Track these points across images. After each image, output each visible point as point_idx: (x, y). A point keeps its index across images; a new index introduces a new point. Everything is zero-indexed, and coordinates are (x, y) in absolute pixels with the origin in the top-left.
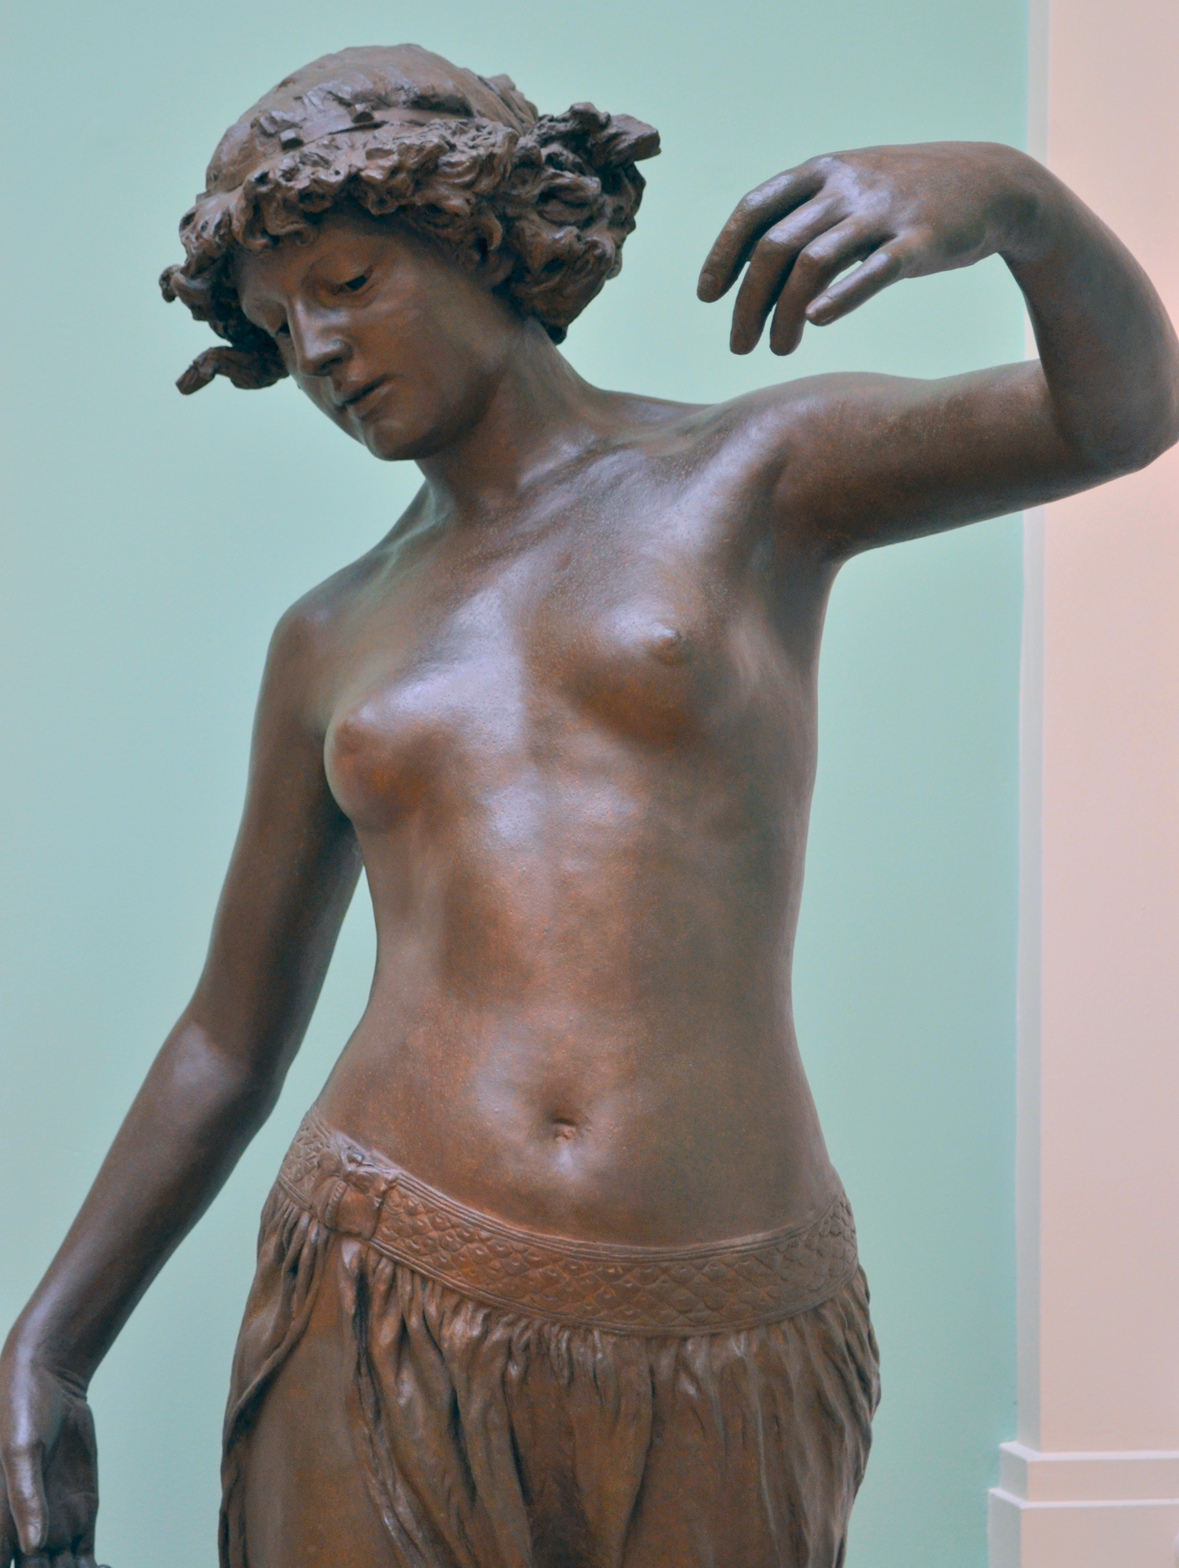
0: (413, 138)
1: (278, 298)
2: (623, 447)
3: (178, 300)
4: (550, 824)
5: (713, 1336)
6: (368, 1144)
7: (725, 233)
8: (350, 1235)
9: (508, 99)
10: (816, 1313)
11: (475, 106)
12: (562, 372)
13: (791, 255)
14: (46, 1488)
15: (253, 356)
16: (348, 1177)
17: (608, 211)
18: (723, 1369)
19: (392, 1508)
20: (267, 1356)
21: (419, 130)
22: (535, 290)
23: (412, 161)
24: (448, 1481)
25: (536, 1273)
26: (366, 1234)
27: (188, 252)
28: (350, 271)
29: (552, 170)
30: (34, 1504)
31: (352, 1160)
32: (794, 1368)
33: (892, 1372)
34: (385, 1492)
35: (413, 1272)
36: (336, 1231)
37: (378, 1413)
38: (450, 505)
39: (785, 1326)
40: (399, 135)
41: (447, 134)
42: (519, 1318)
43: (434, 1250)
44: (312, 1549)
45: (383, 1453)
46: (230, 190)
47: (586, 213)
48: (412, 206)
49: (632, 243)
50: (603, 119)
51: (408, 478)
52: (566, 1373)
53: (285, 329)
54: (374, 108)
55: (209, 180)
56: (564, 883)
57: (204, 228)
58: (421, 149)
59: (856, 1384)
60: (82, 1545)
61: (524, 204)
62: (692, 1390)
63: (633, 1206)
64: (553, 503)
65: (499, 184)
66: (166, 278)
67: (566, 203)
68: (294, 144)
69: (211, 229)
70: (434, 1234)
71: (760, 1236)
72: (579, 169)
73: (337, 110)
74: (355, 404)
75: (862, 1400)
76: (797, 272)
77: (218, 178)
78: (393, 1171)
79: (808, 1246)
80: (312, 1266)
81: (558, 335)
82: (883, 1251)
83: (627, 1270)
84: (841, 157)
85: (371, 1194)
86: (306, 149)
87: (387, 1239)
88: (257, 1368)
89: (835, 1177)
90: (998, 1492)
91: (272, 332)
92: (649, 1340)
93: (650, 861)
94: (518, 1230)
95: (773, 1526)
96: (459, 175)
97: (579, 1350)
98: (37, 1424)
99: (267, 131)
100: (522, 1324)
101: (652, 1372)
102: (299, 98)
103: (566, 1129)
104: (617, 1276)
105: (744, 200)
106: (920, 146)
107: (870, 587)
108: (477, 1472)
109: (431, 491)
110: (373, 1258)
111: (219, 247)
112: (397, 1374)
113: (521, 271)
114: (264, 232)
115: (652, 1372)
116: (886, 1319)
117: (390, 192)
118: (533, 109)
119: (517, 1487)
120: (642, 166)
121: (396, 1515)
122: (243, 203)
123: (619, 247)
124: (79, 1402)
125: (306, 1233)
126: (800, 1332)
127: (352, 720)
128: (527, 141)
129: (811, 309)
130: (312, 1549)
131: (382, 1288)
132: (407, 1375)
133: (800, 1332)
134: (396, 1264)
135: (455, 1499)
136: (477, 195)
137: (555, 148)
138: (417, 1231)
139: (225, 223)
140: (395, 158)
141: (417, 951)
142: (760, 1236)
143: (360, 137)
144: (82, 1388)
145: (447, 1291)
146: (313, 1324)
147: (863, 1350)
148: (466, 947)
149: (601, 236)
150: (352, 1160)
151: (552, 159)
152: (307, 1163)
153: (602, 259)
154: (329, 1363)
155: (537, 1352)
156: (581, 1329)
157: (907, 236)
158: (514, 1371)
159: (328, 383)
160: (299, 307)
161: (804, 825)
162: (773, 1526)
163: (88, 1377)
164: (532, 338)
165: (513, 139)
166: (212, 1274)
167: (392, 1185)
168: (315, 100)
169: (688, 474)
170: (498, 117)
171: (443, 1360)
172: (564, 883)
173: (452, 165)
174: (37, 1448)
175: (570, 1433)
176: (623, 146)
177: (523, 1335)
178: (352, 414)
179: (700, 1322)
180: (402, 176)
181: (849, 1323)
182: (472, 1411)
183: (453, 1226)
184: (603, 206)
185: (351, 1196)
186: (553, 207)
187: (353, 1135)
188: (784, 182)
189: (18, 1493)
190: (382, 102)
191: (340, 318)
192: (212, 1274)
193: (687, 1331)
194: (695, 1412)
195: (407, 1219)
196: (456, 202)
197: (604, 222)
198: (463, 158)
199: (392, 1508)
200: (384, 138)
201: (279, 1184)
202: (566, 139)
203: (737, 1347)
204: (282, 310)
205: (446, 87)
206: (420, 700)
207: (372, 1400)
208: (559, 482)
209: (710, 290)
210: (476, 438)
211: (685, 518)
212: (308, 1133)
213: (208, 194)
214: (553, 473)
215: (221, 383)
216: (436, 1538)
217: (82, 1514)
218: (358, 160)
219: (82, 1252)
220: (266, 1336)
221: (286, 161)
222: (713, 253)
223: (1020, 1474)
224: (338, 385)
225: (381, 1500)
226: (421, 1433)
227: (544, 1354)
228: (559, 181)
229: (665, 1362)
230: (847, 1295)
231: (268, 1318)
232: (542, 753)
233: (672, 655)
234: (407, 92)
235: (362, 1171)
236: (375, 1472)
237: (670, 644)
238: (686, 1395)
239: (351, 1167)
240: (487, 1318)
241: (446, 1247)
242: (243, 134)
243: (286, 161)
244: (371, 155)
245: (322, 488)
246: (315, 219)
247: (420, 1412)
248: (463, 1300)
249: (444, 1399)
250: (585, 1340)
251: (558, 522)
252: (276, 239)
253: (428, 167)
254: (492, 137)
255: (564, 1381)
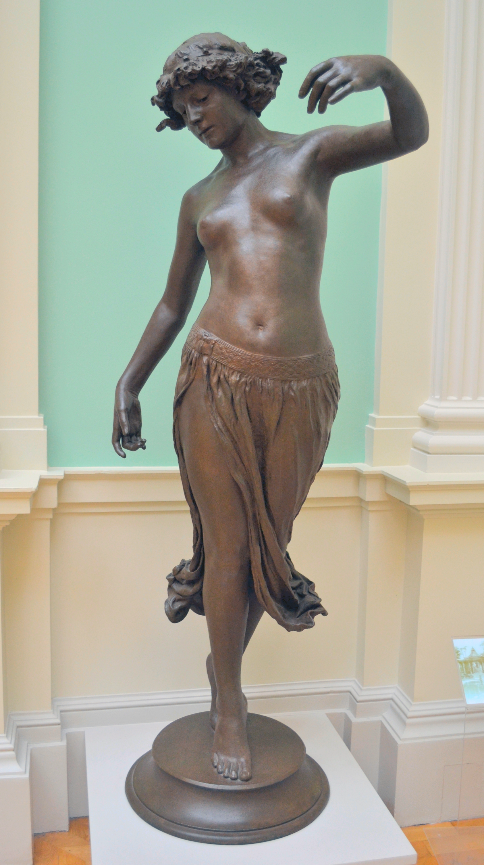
0: (220, 58)
1: (183, 104)
2: (276, 146)
3: (156, 105)
4: (256, 247)
5: (298, 380)
6: (210, 331)
7: (306, 79)
8: (205, 354)
9: (245, 48)
10: (325, 375)
11: (236, 49)
12: (259, 124)
13: (324, 85)
14: (129, 419)
15: (176, 121)
16: (204, 340)
17: (273, 79)
18: (301, 389)
19: (216, 423)
20: (184, 386)
21: (221, 56)
22: (253, 102)
23: (219, 64)
24: (231, 417)
25: (253, 364)
26: (209, 354)
27: (158, 91)
28: (203, 96)
29: (257, 68)
30: (126, 423)
31: (205, 336)
32: (319, 389)
33: (343, 391)
34: (215, 419)
35: (221, 364)
36: (202, 354)
37: (213, 399)
38: (230, 162)
39: (317, 378)
40: (215, 57)
41: (229, 57)
42: (249, 376)
43: (227, 358)
44: (196, 433)
45: (214, 409)
46: (170, 73)
47: (267, 80)
48: (219, 77)
49: (279, 88)
50: (271, 53)
51: (218, 155)
52: (261, 389)
53: (185, 113)
54: (209, 50)
55: (164, 71)
56: (260, 263)
57: (163, 84)
58: (222, 60)
59: (334, 394)
60: (138, 434)
61: (250, 77)
62: (293, 394)
63: (279, 347)
64: (258, 161)
65: (243, 71)
66: (152, 99)
67: (261, 77)
68: (187, 60)
69: (165, 84)
70: (227, 354)
71: (311, 355)
72: (265, 67)
73: (198, 50)
74: (204, 134)
75: (336, 398)
76: (326, 90)
77: (166, 70)
78: (216, 338)
79: (323, 358)
80: (196, 363)
81: (259, 115)
82: (341, 361)
83: (277, 363)
84: (338, 58)
85: (211, 344)
86: (190, 61)
87: (215, 356)
88: (182, 389)
89: (330, 341)
90: (368, 426)
91: (181, 114)
92: (282, 381)
93: (283, 257)
94: (249, 353)
95: (313, 428)
96: (232, 68)
97: (264, 384)
98: (126, 404)
99: (179, 56)
100: (250, 377)
101: (283, 390)
102: (188, 47)
103: (261, 327)
104: (274, 365)
105: (311, 70)
106: (360, 56)
107: (343, 185)
108: (238, 414)
109: (224, 159)
110: (211, 361)
111: (167, 89)
112: (218, 390)
113: (249, 96)
114: (179, 85)
115: (283, 390)
116: (342, 377)
117: (213, 73)
118: (252, 51)
119: (248, 418)
120: (282, 67)
121: (217, 425)
122: (173, 77)
123: (275, 90)
124: (136, 399)
125: (194, 354)
126: (320, 380)
127: (204, 220)
128: (251, 59)
129: (329, 100)
130: (196, 433)
131: (213, 368)
132: (220, 390)
133: (320, 380)
134: (217, 362)
135: (233, 421)
136: (237, 74)
137: (258, 61)
138: (222, 353)
139: (168, 82)
140: (215, 63)
141: (221, 282)
142: (311, 355)
143: (205, 58)
144: (137, 396)
145: (230, 369)
146: (196, 378)
147: (336, 385)
148: (235, 280)
149: (270, 86)
150: (205, 336)
151: (258, 64)
152: (194, 337)
153: (271, 93)
154: (200, 387)
155: (253, 384)
156: (265, 378)
157: (356, 80)
158: (247, 389)
159: (197, 127)
160: (189, 106)
161: (324, 249)
162: (313, 428)
163: (138, 393)
164: (252, 115)
165: (247, 58)
166: (169, 369)
167: (216, 342)
168: (193, 47)
169: (294, 153)
170: (242, 52)
171: (229, 386)
172: (260, 263)
173: (230, 65)
174: (126, 410)
175: (261, 404)
176: (277, 61)
177: (250, 380)
178: (203, 136)
179: (295, 377)
180: (217, 68)
181: (333, 378)
182: (237, 398)
183: (232, 352)
184: (271, 78)
185: (205, 345)
186: (258, 78)
187: (206, 329)
188: (322, 65)
189: (122, 421)
190: (211, 48)
191: (200, 109)
192: (169, 369)
193: (291, 379)
194: (293, 399)
195: (219, 350)
196: (231, 76)
197: (271, 83)
198: (233, 63)
199: (216, 423)
200: (212, 58)
201: (187, 343)
202: (261, 59)
203: (304, 383)
204: (185, 107)
205: (229, 44)
206: (222, 215)
207: (211, 396)
208: (260, 155)
209: (302, 95)
210: (237, 143)
211: (293, 165)
212: (194, 329)
213: (164, 75)
214: (257, 153)
215: (168, 128)
216: (228, 430)
217: (138, 426)
218: (205, 64)
219: (136, 361)
220: (184, 381)
221: (185, 64)
222: (303, 85)
223: (374, 421)
224: (199, 128)
225: (214, 421)
226: (223, 404)
227: (255, 385)
228: (259, 71)
229: (286, 387)
230: (332, 371)
231: (184, 376)
232: (255, 228)
233: (289, 202)
234: (218, 45)
235: (208, 338)
236: (212, 414)
237: (289, 199)
238: (291, 395)
239: (205, 337)
240: (240, 376)
241: (230, 357)
242: (173, 57)
243: (185, 64)
244: (208, 62)
245: (196, 157)
246: (193, 81)
247: (223, 399)
248: (234, 371)
249: (229, 396)
250: (265, 381)
251: (259, 166)
252: (182, 87)
253: (223, 66)
254: (241, 57)
255: (260, 391)
